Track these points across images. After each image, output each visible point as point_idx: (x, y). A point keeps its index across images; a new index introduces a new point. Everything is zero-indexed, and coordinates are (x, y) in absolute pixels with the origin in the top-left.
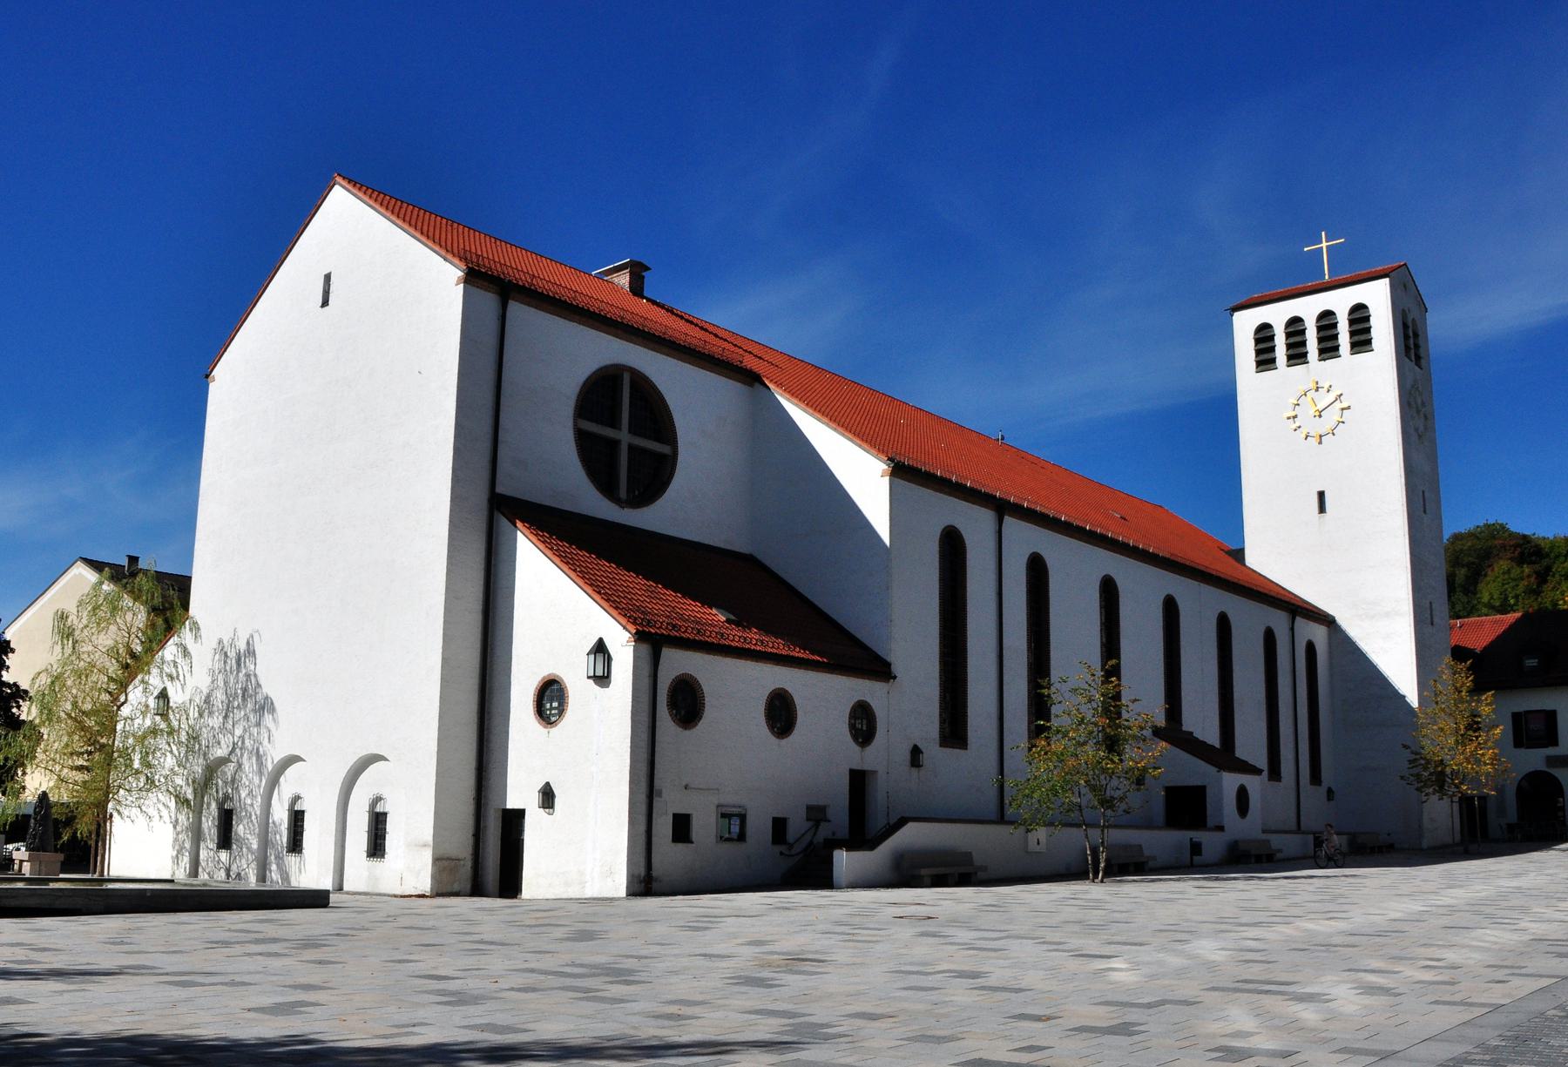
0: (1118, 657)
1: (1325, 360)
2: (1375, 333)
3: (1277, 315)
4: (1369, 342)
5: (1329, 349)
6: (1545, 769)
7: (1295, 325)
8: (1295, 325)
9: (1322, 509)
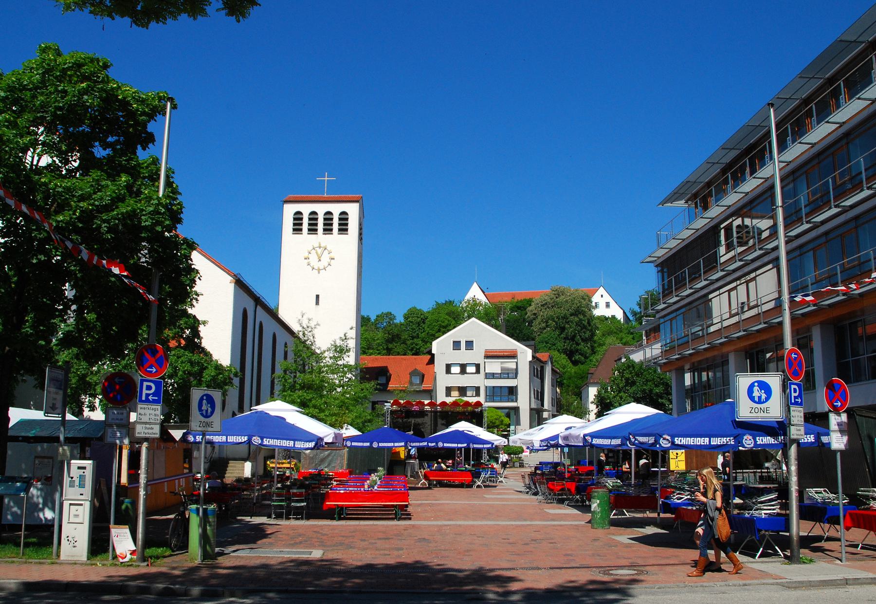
0: (812, 365)
1: (325, 234)
2: (350, 227)
3: (306, 209)
4: (347, 230)
5: (328, 230)
6: (99, 409)
7: (313, 216)
8: (313, 216)
9: (317, 303)
